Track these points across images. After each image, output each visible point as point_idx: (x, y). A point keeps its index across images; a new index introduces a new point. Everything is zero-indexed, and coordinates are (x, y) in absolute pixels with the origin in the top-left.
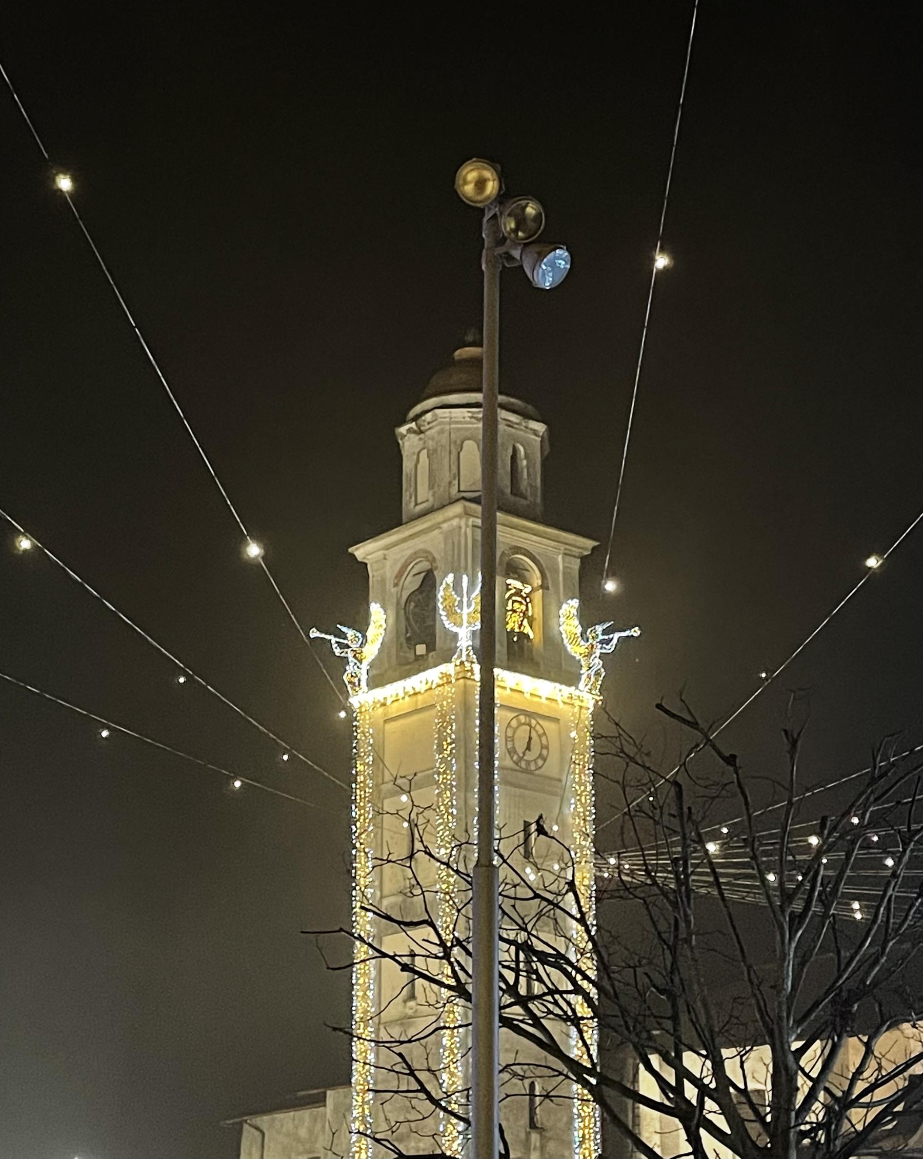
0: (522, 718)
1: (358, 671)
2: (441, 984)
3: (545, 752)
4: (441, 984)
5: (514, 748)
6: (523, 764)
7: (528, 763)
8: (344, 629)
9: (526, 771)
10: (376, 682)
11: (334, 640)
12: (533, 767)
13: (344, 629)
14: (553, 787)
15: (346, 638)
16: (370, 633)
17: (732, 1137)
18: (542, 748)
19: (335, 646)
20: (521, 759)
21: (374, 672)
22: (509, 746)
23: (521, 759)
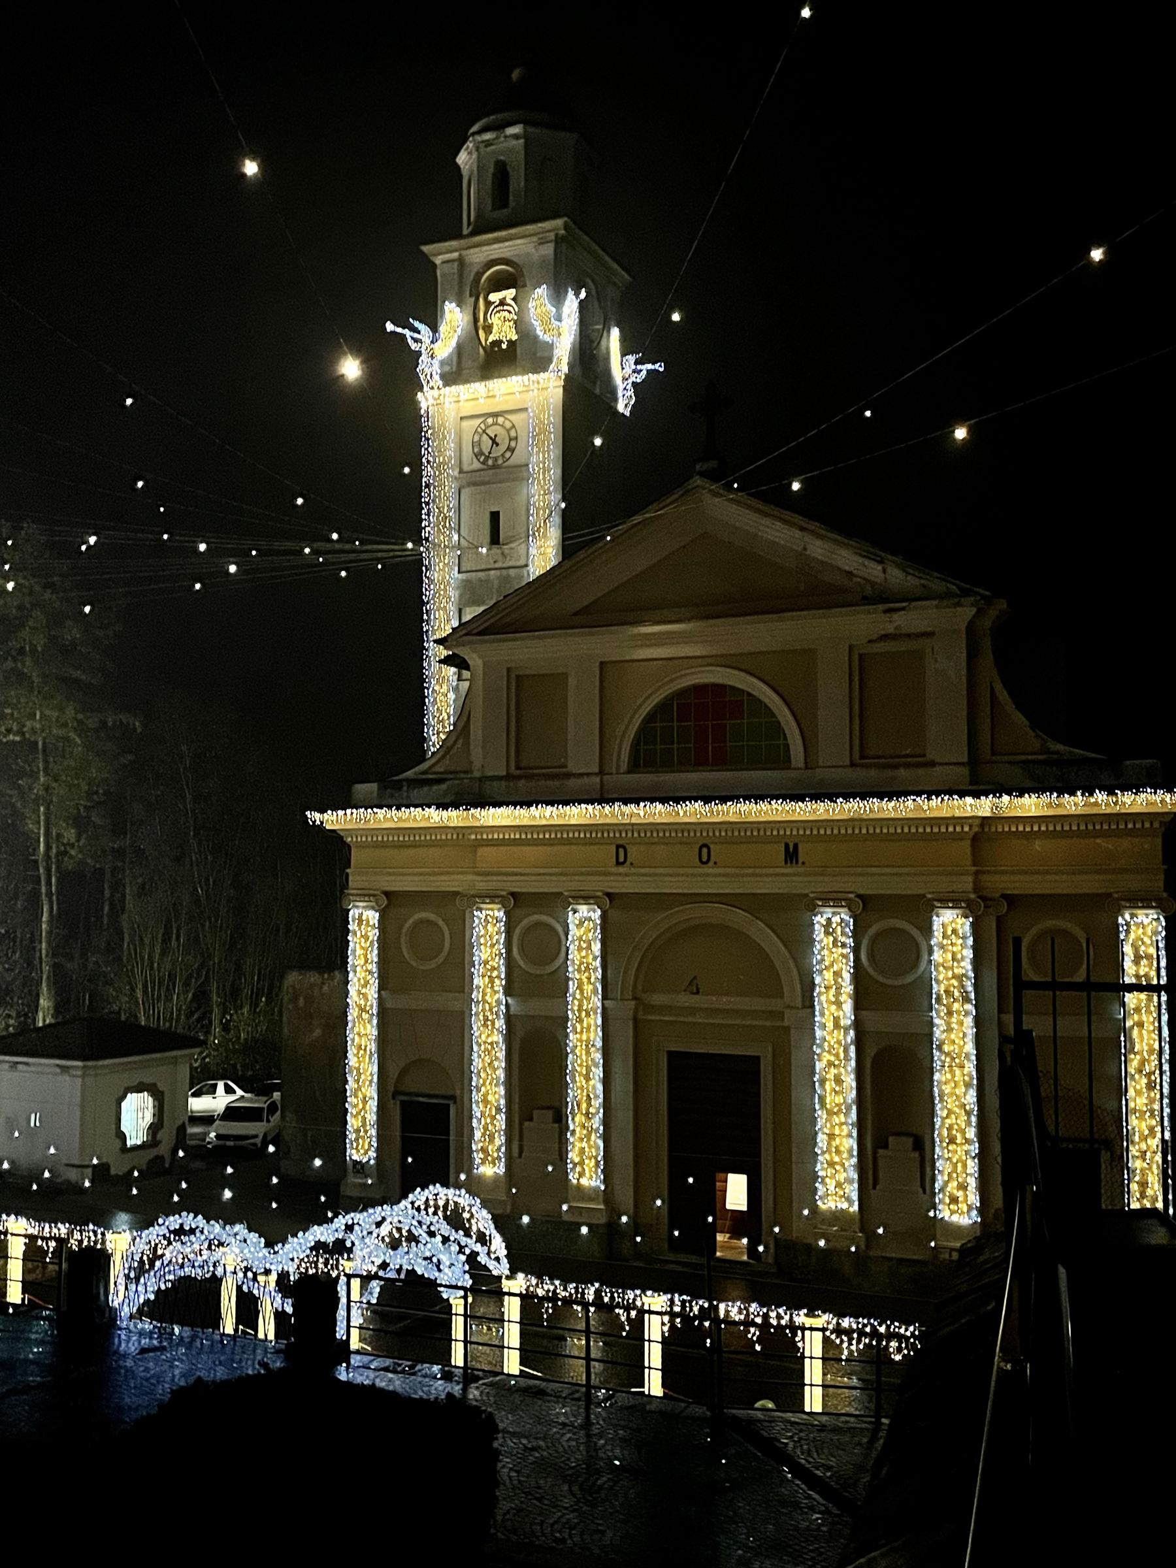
0: (490, 421)
1: (429, 369)
2: (446, 1286)
3: (513, 444)
4: (446, 1286)
5: (481, 450)
6: (490, 462)
7: (496, 459)
8: (417, 324)
9: (495, 467)
10: (450, 378)
11: (407, 332)
12: (500, 462)
13: (417, 324)
14: (519, 473)
15: (419, 332)
16: (443, 328)
17: (21, 581)
18: (510, 440)
19: (409, 340)
20: (487, 458)
21: (447, 368)
22: (476, 450)
23: (487, 458)
